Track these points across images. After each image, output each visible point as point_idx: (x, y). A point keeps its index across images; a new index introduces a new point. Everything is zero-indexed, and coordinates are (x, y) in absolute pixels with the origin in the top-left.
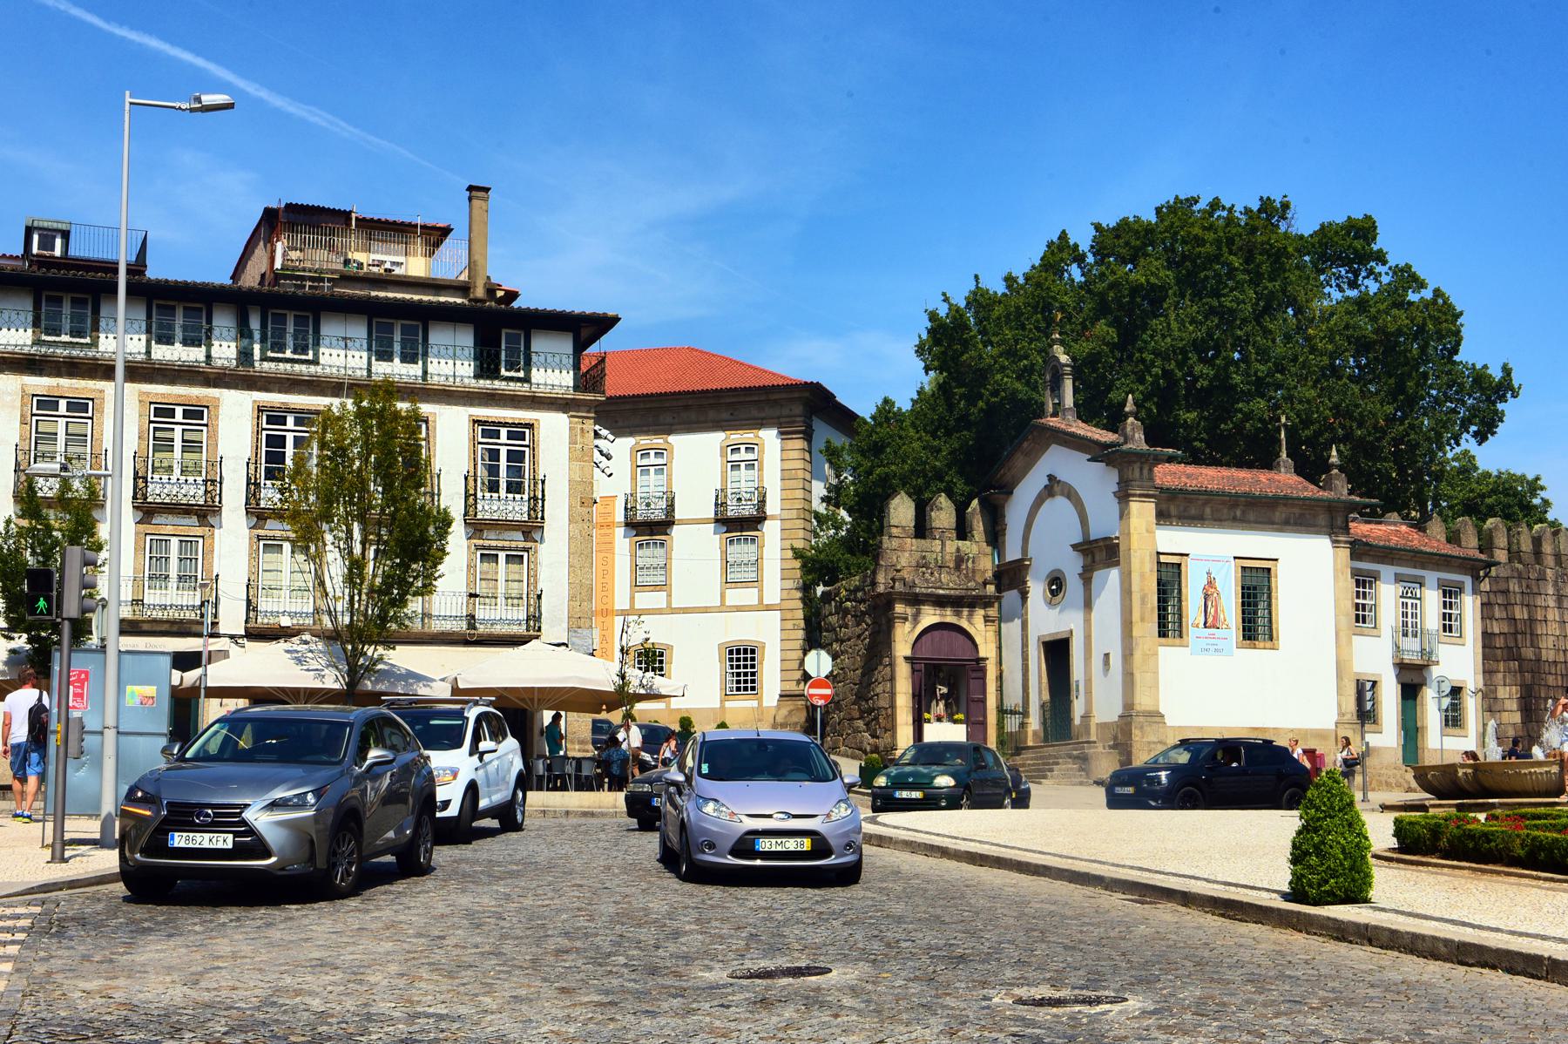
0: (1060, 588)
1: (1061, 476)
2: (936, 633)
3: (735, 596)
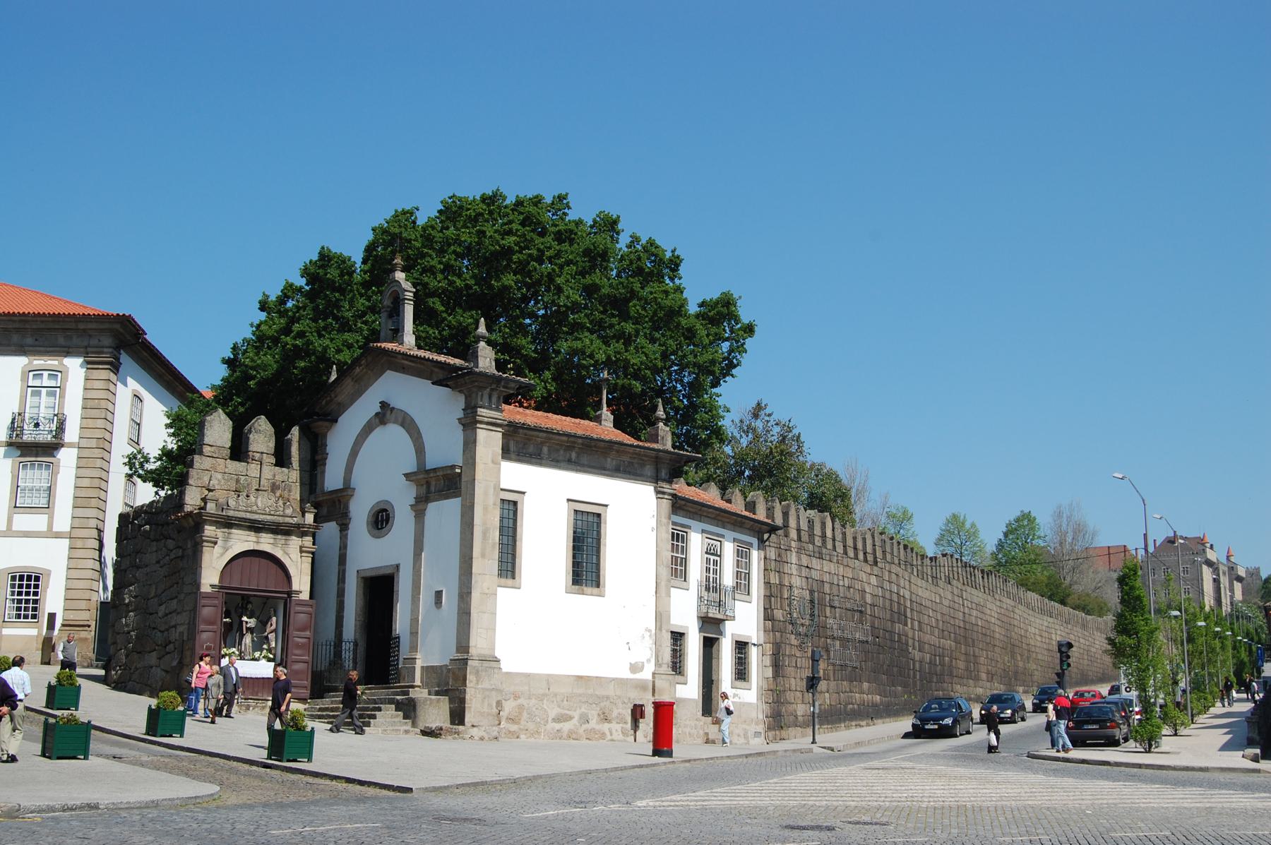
1: (396, 403)
2: (240, 560)
3: (24, 522)
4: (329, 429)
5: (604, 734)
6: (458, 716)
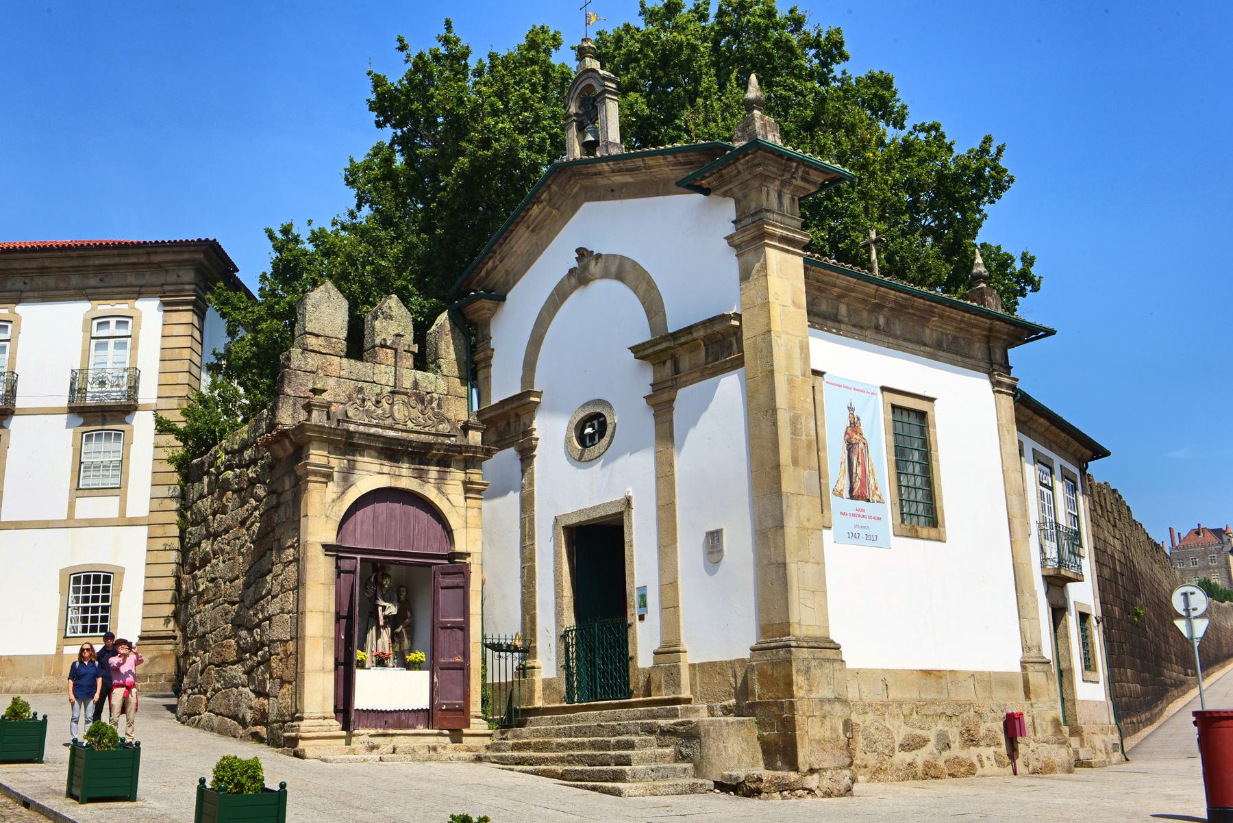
0: (602, 430)
2: (382, 507)
3: (88, 507)
4: (493, 312)
5: (972, 765)
6: (781, 749)
